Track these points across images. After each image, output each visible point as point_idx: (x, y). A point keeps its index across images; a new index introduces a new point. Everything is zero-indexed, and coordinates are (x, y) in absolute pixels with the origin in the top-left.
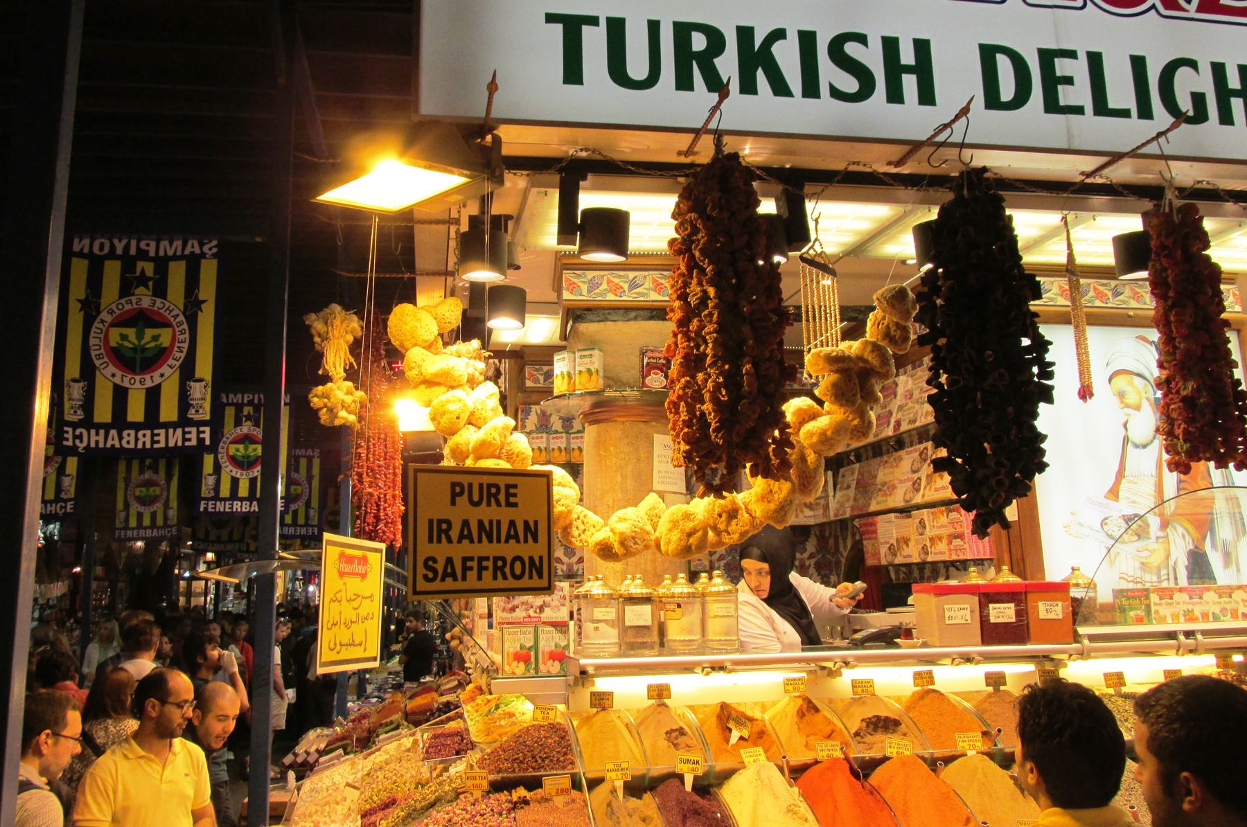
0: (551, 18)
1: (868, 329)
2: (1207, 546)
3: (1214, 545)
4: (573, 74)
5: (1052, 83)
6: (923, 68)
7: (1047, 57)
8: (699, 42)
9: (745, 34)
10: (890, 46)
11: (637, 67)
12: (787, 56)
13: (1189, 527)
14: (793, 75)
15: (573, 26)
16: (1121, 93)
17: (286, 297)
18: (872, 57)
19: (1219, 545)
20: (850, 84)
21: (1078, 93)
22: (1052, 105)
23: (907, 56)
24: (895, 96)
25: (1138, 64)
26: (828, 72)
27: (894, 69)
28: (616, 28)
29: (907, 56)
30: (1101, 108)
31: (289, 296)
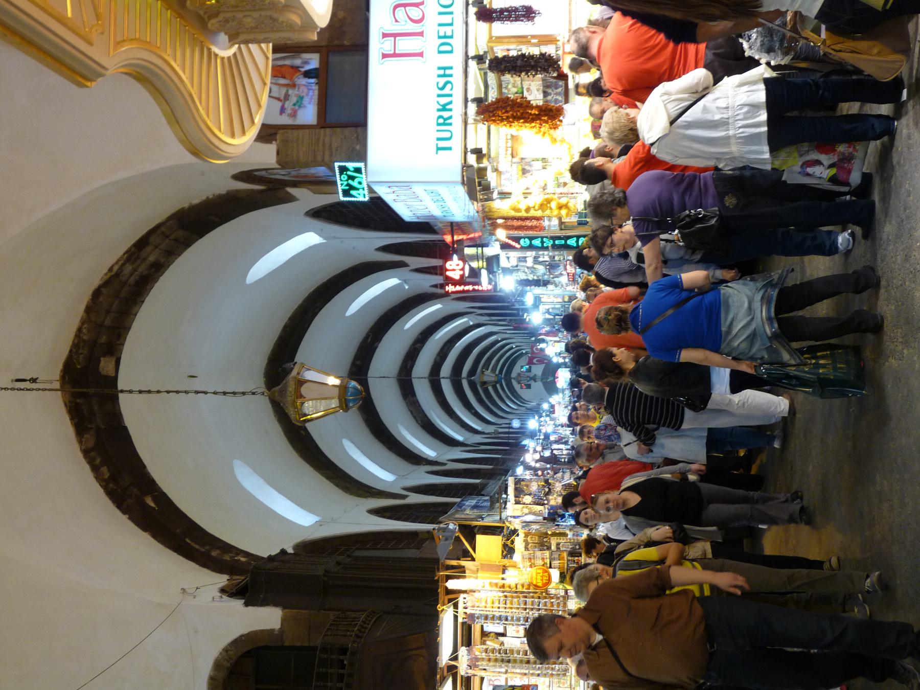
0: (437, 153)
1: (345, 679)
2: (303, 70)
3: (302, 67)
4: (450, 149)
5: (445, 37)
6: (445, 68)
7: (440, 37)
8: (441, 121)
9: (438, 110)
10: (439, 76)
11: (447, 135)
12: (443, 101)
13: (295, 76)
14: (447, 100)
15: (439, 149)
16: (447, 19)
17: (795, 649)
18: (442, 81)
19: (302, 65)
20: (449, 86)
21: (448, 30)
22: (451, 37)
23: (442, 72)
24: (451, 76)
25: (440, 13)
26: (447, 91)
27: (444, 75)
28: (439, 139)
29: (442, 72)
30: (451, 24)
31: (796, 653)
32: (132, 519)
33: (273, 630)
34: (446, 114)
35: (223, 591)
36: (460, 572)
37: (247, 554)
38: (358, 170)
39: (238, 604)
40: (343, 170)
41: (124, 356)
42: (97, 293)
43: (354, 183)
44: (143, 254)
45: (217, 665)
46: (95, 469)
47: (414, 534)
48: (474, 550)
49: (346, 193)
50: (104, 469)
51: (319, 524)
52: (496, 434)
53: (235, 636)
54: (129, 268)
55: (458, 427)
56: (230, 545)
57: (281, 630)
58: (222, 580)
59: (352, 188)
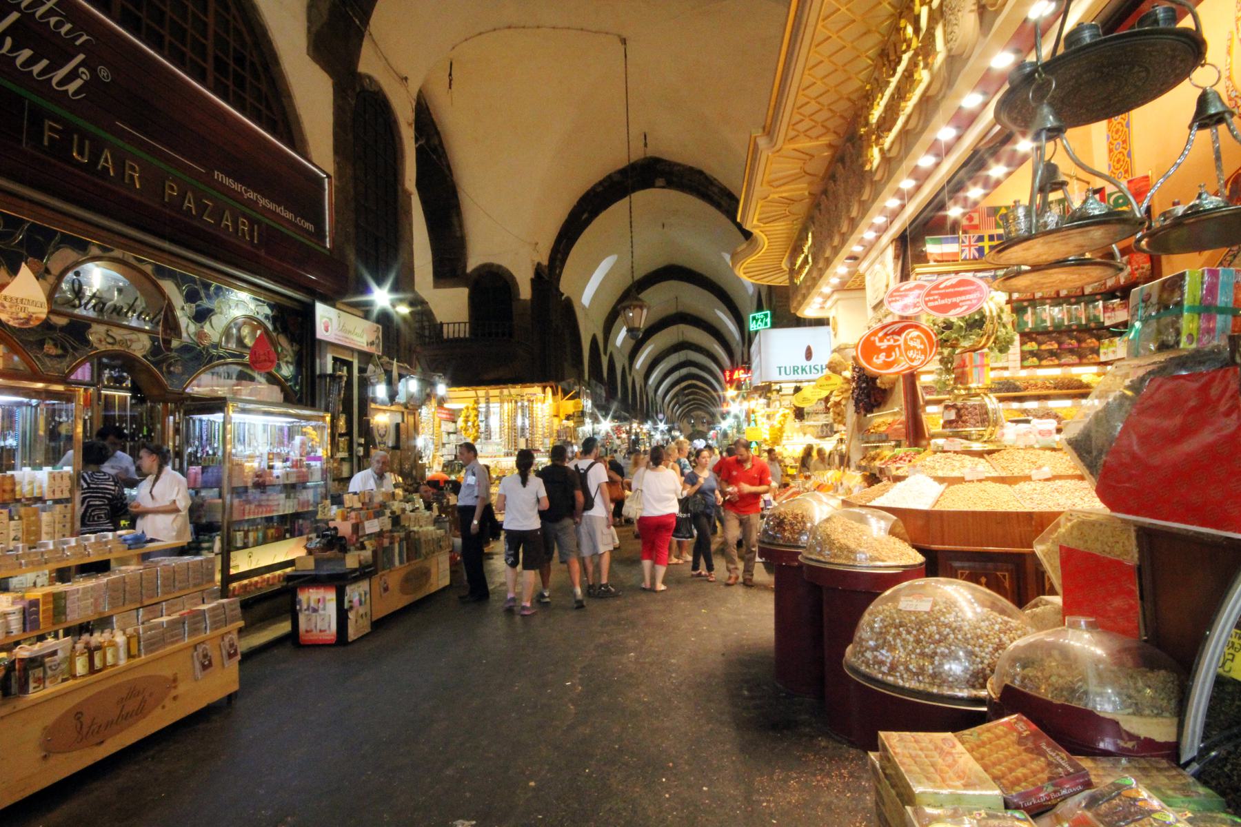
11: (788, 372)
12: (807, 369)
26: (813, 370)
32: (575, 207)
33: (519, 294)
34: (800, 371)
35: (539, 264)
36: (554, 394)
37: (561, 273)
38: (766, 324)
39: (531, 274)
40: (766, 315)
41: (666, 191)
42: (701, 173)
43: (759, 322)
44: (725, 198)
45: (499, 267)
46: (601, 183)
47: (581, 362)
48: (568, 399)
49: (754, 318)
50: (601, 189)
51: (584, 308)
52: (654, 403)
53: (515, 274)
54: (716, 190)
55: (657, 382)
56: (576, 240)
57: (519, 300)
58: (545, 262)
59: (757, 321)
